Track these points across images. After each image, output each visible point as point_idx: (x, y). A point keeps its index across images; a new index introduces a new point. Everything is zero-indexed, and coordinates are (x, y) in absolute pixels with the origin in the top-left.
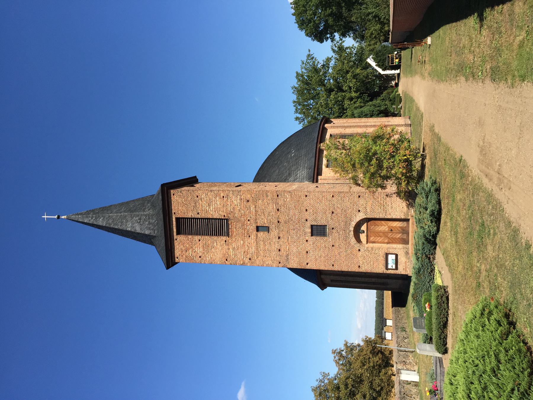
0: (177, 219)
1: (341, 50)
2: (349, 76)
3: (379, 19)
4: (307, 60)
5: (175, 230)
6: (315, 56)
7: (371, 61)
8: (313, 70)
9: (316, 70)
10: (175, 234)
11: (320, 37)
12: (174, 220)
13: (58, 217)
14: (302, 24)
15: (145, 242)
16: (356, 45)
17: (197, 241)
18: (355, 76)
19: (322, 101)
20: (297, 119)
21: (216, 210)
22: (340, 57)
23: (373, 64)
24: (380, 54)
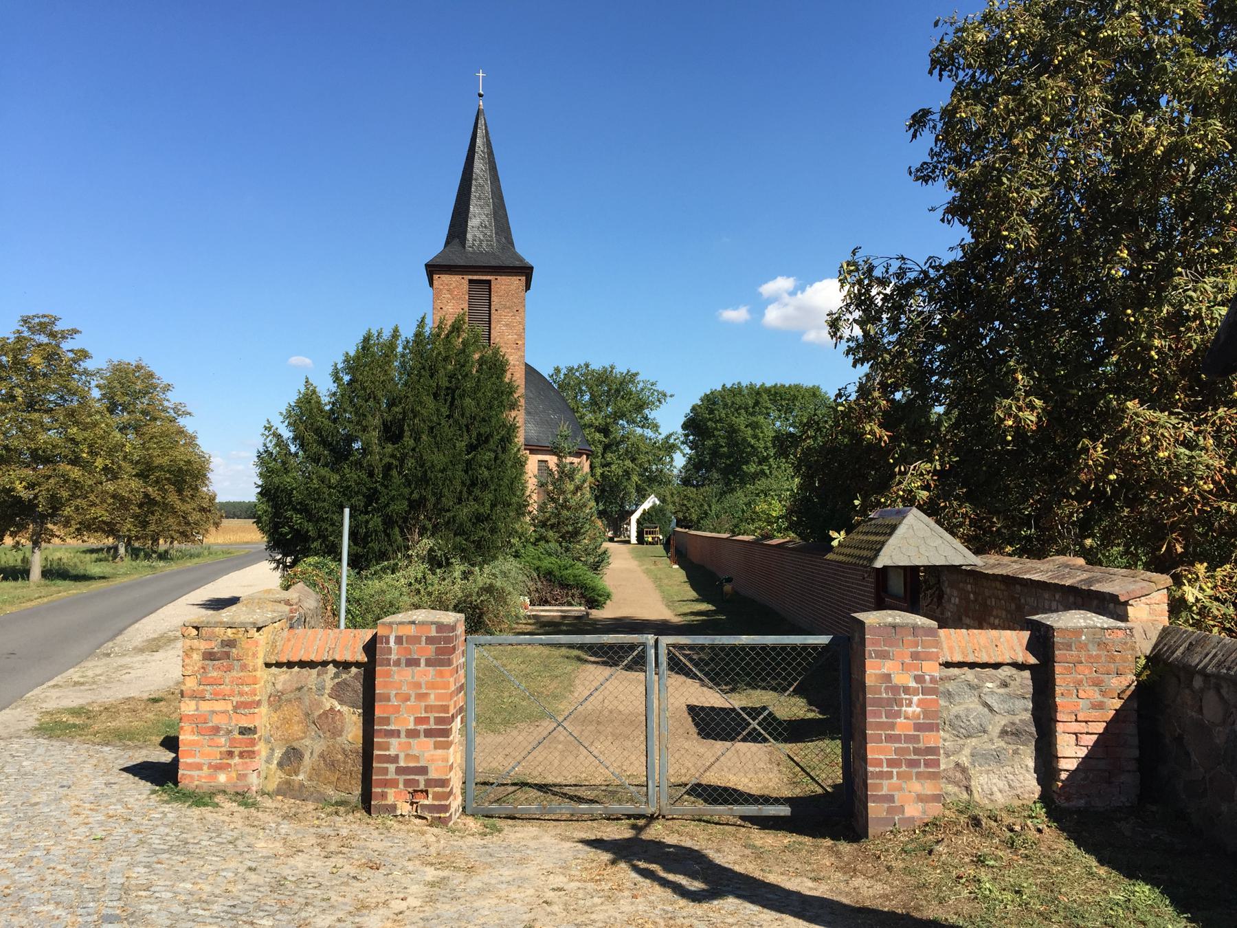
0: (489, 282)
1: (670, 448)
2: (628, 463)
3: (702, 518)
4: (657, 391)
5: (475, 277)
6: (664, 406)
7: (650, 502)
8: (640, 403)
9: (640, 407)
10: (470, 277)
11: (694, 424)
12: (488, 278)
13: (480, 95)
14: (710, 401)
15: (452, 226)
16: (676, 472)
17: (462, 306)
18: (627, 473)
19: (589, 417)
20: (558, 370)
21: (502, 333)
22: (658, 447)
23: (647, 505)
24: (660, 515)
